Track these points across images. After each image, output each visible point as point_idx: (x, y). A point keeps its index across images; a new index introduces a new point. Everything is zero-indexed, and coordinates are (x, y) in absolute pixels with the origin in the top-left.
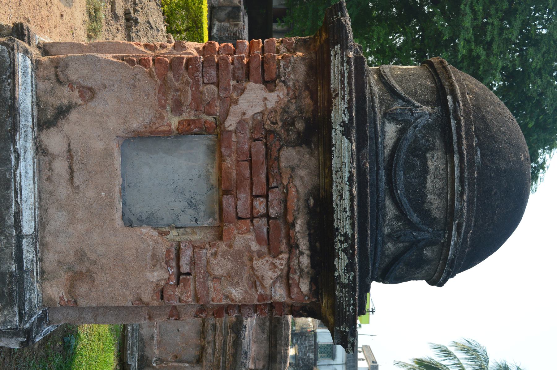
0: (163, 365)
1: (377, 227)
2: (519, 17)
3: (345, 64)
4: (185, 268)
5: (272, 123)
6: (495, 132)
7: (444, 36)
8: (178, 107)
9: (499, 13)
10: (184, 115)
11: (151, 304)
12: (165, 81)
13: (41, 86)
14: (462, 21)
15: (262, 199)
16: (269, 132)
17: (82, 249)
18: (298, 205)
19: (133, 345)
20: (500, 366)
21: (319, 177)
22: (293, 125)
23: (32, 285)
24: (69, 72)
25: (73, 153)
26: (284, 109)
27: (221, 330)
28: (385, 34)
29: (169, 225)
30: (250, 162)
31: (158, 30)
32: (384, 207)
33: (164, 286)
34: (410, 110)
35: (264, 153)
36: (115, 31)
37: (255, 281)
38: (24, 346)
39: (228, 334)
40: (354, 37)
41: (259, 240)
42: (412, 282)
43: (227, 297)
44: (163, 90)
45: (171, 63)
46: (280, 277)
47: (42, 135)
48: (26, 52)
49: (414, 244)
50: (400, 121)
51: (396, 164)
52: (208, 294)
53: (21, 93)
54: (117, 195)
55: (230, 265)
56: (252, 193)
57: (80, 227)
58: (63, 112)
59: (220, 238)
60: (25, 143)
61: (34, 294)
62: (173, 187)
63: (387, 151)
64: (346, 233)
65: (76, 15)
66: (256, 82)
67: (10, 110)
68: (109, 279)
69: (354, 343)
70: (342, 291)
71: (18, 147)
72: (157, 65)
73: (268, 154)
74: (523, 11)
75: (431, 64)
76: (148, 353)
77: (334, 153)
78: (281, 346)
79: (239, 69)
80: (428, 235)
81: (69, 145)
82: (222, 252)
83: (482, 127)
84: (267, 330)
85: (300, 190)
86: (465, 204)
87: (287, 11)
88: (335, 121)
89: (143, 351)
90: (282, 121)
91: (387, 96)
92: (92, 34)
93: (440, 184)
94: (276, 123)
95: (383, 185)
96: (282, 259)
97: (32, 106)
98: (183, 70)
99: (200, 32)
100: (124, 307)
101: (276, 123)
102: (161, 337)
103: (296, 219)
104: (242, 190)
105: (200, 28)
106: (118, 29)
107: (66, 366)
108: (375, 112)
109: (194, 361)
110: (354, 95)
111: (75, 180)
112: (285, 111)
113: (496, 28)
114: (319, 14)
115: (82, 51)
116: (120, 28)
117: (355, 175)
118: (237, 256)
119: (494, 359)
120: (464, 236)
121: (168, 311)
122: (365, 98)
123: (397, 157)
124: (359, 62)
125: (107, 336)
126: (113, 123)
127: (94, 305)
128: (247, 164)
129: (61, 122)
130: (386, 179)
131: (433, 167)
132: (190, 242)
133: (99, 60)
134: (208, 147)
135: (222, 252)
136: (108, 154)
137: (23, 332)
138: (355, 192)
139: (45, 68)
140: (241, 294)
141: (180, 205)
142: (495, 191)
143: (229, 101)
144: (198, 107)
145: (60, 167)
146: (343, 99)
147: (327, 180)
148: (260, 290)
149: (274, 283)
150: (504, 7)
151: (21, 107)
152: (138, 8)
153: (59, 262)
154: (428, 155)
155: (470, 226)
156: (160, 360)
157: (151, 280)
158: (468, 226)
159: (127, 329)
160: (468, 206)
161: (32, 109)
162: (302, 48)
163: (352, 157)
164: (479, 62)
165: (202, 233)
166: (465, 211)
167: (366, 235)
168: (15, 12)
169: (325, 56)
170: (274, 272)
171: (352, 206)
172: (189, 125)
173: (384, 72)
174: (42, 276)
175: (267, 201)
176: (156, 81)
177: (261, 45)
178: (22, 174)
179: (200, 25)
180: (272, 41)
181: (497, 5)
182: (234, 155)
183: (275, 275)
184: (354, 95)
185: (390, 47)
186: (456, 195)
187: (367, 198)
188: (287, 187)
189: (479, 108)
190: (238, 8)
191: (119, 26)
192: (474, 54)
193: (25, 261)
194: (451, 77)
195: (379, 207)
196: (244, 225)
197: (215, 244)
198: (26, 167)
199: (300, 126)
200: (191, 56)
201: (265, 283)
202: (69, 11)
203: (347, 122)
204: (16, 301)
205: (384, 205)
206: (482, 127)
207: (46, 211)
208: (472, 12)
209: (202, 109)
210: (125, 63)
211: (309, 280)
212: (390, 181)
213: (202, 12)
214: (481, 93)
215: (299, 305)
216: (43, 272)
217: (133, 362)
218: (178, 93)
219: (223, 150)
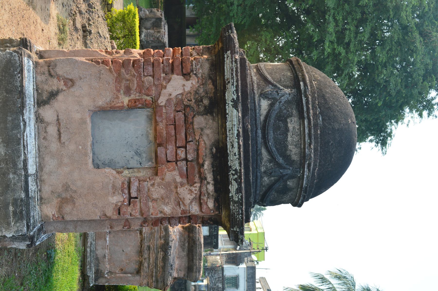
0: (113, 276)
1: (257, 166)
2: (369, 25)
3: (234, 63)
4: (134, 194)
5: (189, 100)
6: (331, 105)
7: (314, 38)
8: (128, 91)
9: (355, 21)
10: (132, 96)
11: (112, 217)
12: (119, 74)
13: (39, 78)
14: (327, 27)
15: (182, 149)
16: (186, 106)
17: (67, 183)
19: (91, 262)
20: (364, 289)
22: (202, 101)
23: (35, 206)
24: (57, 69)
25: (60, 121)
26: (196, 92)
27: (154, 249)
28: (271, 37)
29: (123, 167)
30: (175, 125)
31: (105, 38)
32: (261, 154)
33: (121, 206)
34: (277, 92)
35: (183, 119)
36: (76, 39)
37: (179, 202)
38: (29, 247)
39: (158, 252)
40: (239, 47)
41: (181, 175)
42: (282, 205)
43: (161, 212)
44: (118, 80)
45: (123, 63)
46: (195, 198)
47: (40, 110)
48: (29, 57)
49: (281, 177)
50: (270, 98)
51: (268, 126)
52: (149, 210)
53: (26, 83)
54: (89, 148)
55: (162, 191)
56: (176, 145)
57: (65, 169)
58: (53, 95)
59: (156, 174)
60: (29, 115)
61: (36, 213)
62: (126, 142)
63: (262, 118)
64: (236, 169)
65: (51, 29)
66: (178, 75)
67: (20, 94)
68: (85, 202)
69: (242, 239)
70: (234, 206)
71: (25, 118)
72: (114, 64)
74: (372, 20)
75: (291, 62)
76: (101, 267)
77: (228, 119)
78: (196, 260)
79: (167, 66)
80: (289, 172)
81: (58, 116)
82: (157, 183)
83: (323, 102)
84: (186, 250)
85: (206, 142)
86: (313, 151)
87: (197, 21)
88: (228, 99)
89: (98, 266)
90: (194, 99)
91: (262, 83)
92: (61, 42)
93: (296, 138)
94: (191, 101)
95: (260, 140)
96: (196, 187)
97: (34, 91)
99: (133, 38)
100: (94, 220)
101: (191, 101)
102: (111, 256)
103: (204, 161)
104: (170, 143)
105: (133, 35)
106: (78, 38)
107: (49, 270)
108: (254, 93)
109: (135, 273)
110: (240, 82)
111: (62, 138)
112: (196, 92)
113: (352, 33)
114: (221, 23)
115: (65, 56)
116: (79, 37)
117: (241, 132)
118: (167, 186)
119: (360, 283)
120: (313, 172)
121: (123, 222)
122: (247, 84)
123: (268, 122)
124: (243, 61)
125: (74, 254)
126: (86, 101)
127: (75, 219)
128: (173, 126)
130: (262, 136)
131: (292, 128)
132: (137, 177)
133: (77, 61)
134: (148, 116)
135: (157, 183)
136: (83, 122)
137: (29, 238)
138: (241, 143)
139: (41, 67)
140: (170, 210)
141: (130, 154)
142: (332, 142)
143: (161, 87)
144: (141, 91)
145: (52, 130)
146: (233, 85)
147: (224, 136)
148: (182, 207)
149: (191, 202)
150: (358, 17)
151: (27, 92)
152: (91, 23)
153: (52, 192)
154: (289, 120)
155: (316, 165)
156: (110, 272)
158: (315, 165)
159: (87, 250)
160: (314, 152)
161: (34, 93)
162: (207, 52)
163: (239, 121)
164: (341, 58)
165: (145, 172)
166: (312, 156)
167: (249, 171)
168: (16, 29)
169: (221, 57)
170: (191, 195)
171: (239, 151)
172: (135, 102)
173: (260, 67)
176: (113, 75)
177: (180, 51)
178: (28, 135)
179: (133, 33)
180: (188, 48)
181: (353, 16)
182: (164, 121)
183: (192, 197)
184: (240, 82)
185: (274, 47)
186: (306, 145)
187: (249, 147)
188: (198, 141)
189: (321, 90)
190: (160, 19)
191: (78, 36)
192: (337, 52)
193: (30, 191)
194: (303, 70)
195: (257, 154)
196: (171, 166)
197: (153, 178)
198: (30, 131)
199: (206, 102)
200: (136, 58)
201: (185, 202)
202: (47, 27)
203: (235, 99)
204: (25, 217)
205: (261, 152)
206: (323, 102)
207: (43, 159)
208: (334, 21)
209: (144, 92)
210: (94, 63)
211: (214, 200)
213: (135, 24)
214: (323, 80)
215: (207, 217)
216: (41, 199)
218: (128, 82)
219: (157, 118)
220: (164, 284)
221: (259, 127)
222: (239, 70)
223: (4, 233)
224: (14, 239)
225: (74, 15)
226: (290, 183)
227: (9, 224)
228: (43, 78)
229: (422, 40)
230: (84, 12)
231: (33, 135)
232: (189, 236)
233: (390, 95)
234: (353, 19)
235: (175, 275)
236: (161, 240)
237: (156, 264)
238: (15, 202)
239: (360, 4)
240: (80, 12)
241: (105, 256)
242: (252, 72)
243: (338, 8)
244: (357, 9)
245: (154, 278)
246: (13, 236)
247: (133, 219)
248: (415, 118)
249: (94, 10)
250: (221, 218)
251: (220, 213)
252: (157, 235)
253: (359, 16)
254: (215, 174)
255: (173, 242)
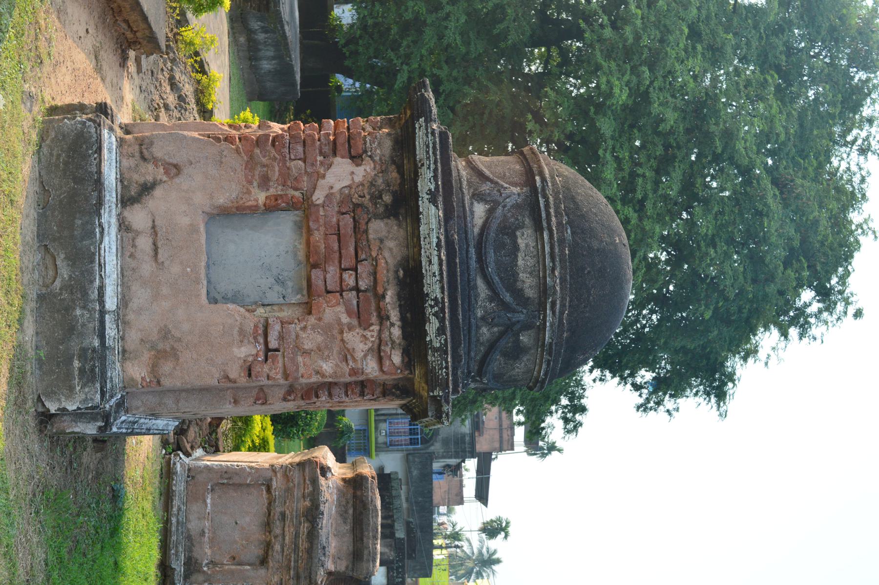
1: (469, 309)
3: (430, 135)
5: (360, 196)
8: (265, 182)
9: (652, 160)
12: (251, 157)
17: (165, 326)
18: (388, 277)
21: (408, 247)
22: (380, 197)
24: (154, 150)
25: (158, 229)
26: (371, 183)
27: (292, 519)
30: (339, 235)
34: (499, 191)
35: (352, 226)
37: (346, 355)
39: (300, 524)
41: (349, 313)
43: (317, 373)
45: (257, 141)
48: (111, 129)
51: (486, 242)
53: (106, 169)
55: (320, 339)
57: (164, 303)
58: (147, 189)
59: (310, 313)
60: (109, 217)
61: (115, 373)
62: (260, 263)
63: (476, 230)
66: (343, 157)
68: (195, 356)
70: (434, 355)
73: (356, 228)
78: (369, 538)
79: (325, 145)
80: (522, 317)
81: (154, 221)
85: (389, 261)
86: (558, 281)
89: (191, 551)
90: (369, 194)
91: (475, 179)
93: (531, 262)
95: (473, 264)
96: (373, 331)
98: (269, 147)
102: (214, 533)
103: (386, 290)
108: (463, 193)
109: (258, 563)
111: (160, 256)
112: (372, 184)
118: (327, 330)
121: (254, 393)
126: (199, 198)
128: (335, 237)
129: (145, 199)
133: (185, 137)
134: (295, 223)
137: (102, 416)
138: (444, 258)
139: (129, 146)
145: (144, 243)
146: (429, 168)
147: (416, 250)
148: (351, 363)
149: (365, 356)
150: (658, 153)
151: (106, 183)
153: (142, 340)
154: (518, 233)
156: (212, 563)
157: (239, 356)
158: (563, 305)
160: (561, 284)
166: (558, 288)
167: (457, 305)
170: (365, 344)
171: (441, 270)
172: (276, 200)
174: (123, 356)
175: (357, 274)
177: (346, 125)
182: (322, 229)
183: (367, 347)
189: (568, 189)
195: (469, 287)
196: (333, 298)
199: (387, 198)
201: (356, 355)
204: (98, 378)
205: (476, 284)
207: (129, 288)
209: (289, 184)
212: (481, 260)
216: (124, 351)
217: (178, 566)
218: (265, 169)
219: (311, 224)
220: (310, 581)
221: (472, 243)
222: (438, 147)
223: (64, 405)
224: (78, 415)
225: (156, 109)
226: (524, 338)
227: (71, 389)
228: (132, 162)
229: (777, 193)
230: (172, 107)
231: (114, 250)
232: (355, 496)
233: (726, 299)
234: (649, 157)
235: (330, 566)
236: (305, 501)
237: (296, 548)
238: (83, 354)
239: (660, 129)
240: (166, 107)
241: (204, 532)
242: (459, 165)
243: (620, 137)
244: (656, 140)
245: (292, 572)
246: (79, 408)
247: (272, 386)
248: (780, 351)
249: (187, 106)
250: (413, 384)
251: (411, 373)
252: (297, 493)
253: (659, 151)
254: (402, 309)
255: (327, 504)
